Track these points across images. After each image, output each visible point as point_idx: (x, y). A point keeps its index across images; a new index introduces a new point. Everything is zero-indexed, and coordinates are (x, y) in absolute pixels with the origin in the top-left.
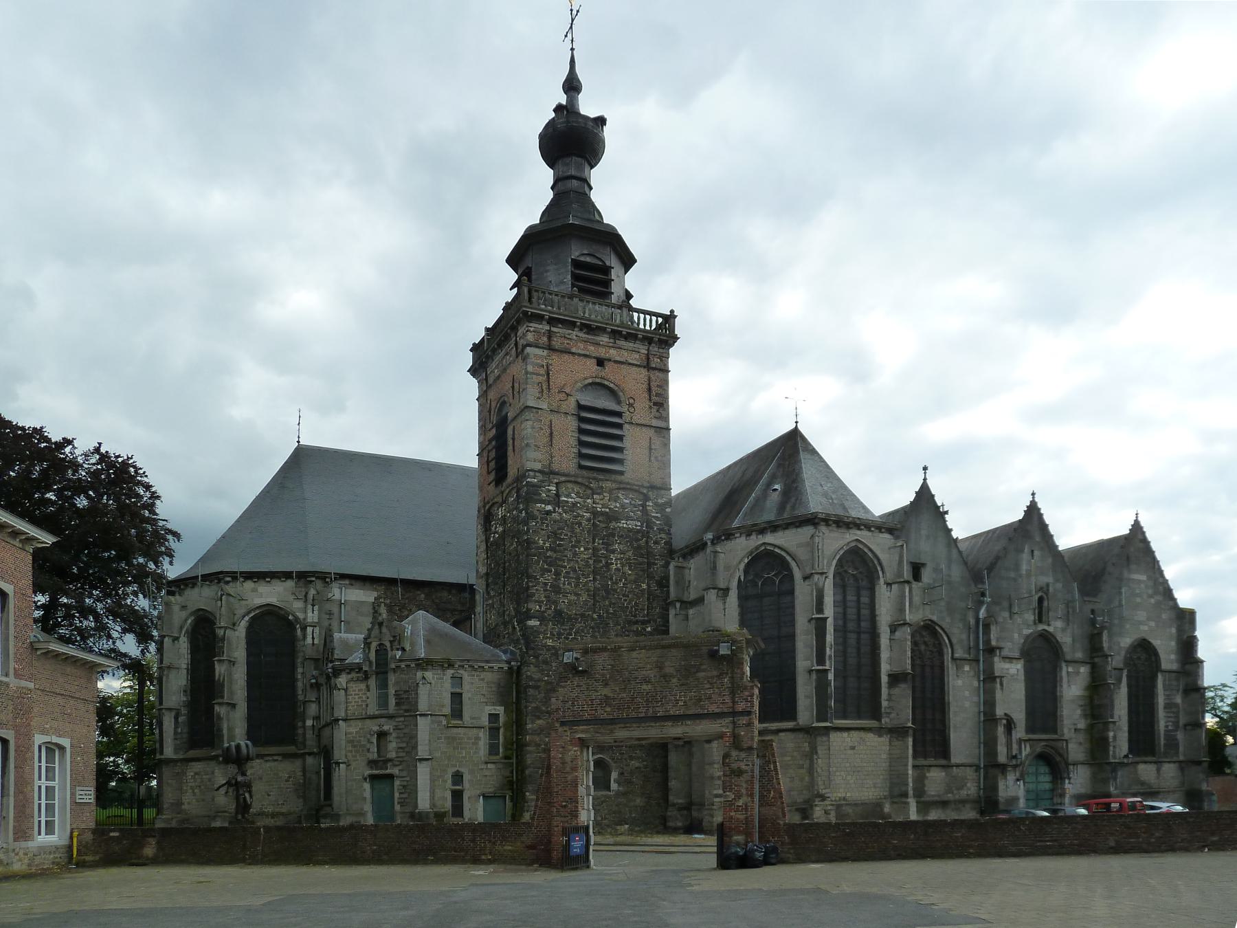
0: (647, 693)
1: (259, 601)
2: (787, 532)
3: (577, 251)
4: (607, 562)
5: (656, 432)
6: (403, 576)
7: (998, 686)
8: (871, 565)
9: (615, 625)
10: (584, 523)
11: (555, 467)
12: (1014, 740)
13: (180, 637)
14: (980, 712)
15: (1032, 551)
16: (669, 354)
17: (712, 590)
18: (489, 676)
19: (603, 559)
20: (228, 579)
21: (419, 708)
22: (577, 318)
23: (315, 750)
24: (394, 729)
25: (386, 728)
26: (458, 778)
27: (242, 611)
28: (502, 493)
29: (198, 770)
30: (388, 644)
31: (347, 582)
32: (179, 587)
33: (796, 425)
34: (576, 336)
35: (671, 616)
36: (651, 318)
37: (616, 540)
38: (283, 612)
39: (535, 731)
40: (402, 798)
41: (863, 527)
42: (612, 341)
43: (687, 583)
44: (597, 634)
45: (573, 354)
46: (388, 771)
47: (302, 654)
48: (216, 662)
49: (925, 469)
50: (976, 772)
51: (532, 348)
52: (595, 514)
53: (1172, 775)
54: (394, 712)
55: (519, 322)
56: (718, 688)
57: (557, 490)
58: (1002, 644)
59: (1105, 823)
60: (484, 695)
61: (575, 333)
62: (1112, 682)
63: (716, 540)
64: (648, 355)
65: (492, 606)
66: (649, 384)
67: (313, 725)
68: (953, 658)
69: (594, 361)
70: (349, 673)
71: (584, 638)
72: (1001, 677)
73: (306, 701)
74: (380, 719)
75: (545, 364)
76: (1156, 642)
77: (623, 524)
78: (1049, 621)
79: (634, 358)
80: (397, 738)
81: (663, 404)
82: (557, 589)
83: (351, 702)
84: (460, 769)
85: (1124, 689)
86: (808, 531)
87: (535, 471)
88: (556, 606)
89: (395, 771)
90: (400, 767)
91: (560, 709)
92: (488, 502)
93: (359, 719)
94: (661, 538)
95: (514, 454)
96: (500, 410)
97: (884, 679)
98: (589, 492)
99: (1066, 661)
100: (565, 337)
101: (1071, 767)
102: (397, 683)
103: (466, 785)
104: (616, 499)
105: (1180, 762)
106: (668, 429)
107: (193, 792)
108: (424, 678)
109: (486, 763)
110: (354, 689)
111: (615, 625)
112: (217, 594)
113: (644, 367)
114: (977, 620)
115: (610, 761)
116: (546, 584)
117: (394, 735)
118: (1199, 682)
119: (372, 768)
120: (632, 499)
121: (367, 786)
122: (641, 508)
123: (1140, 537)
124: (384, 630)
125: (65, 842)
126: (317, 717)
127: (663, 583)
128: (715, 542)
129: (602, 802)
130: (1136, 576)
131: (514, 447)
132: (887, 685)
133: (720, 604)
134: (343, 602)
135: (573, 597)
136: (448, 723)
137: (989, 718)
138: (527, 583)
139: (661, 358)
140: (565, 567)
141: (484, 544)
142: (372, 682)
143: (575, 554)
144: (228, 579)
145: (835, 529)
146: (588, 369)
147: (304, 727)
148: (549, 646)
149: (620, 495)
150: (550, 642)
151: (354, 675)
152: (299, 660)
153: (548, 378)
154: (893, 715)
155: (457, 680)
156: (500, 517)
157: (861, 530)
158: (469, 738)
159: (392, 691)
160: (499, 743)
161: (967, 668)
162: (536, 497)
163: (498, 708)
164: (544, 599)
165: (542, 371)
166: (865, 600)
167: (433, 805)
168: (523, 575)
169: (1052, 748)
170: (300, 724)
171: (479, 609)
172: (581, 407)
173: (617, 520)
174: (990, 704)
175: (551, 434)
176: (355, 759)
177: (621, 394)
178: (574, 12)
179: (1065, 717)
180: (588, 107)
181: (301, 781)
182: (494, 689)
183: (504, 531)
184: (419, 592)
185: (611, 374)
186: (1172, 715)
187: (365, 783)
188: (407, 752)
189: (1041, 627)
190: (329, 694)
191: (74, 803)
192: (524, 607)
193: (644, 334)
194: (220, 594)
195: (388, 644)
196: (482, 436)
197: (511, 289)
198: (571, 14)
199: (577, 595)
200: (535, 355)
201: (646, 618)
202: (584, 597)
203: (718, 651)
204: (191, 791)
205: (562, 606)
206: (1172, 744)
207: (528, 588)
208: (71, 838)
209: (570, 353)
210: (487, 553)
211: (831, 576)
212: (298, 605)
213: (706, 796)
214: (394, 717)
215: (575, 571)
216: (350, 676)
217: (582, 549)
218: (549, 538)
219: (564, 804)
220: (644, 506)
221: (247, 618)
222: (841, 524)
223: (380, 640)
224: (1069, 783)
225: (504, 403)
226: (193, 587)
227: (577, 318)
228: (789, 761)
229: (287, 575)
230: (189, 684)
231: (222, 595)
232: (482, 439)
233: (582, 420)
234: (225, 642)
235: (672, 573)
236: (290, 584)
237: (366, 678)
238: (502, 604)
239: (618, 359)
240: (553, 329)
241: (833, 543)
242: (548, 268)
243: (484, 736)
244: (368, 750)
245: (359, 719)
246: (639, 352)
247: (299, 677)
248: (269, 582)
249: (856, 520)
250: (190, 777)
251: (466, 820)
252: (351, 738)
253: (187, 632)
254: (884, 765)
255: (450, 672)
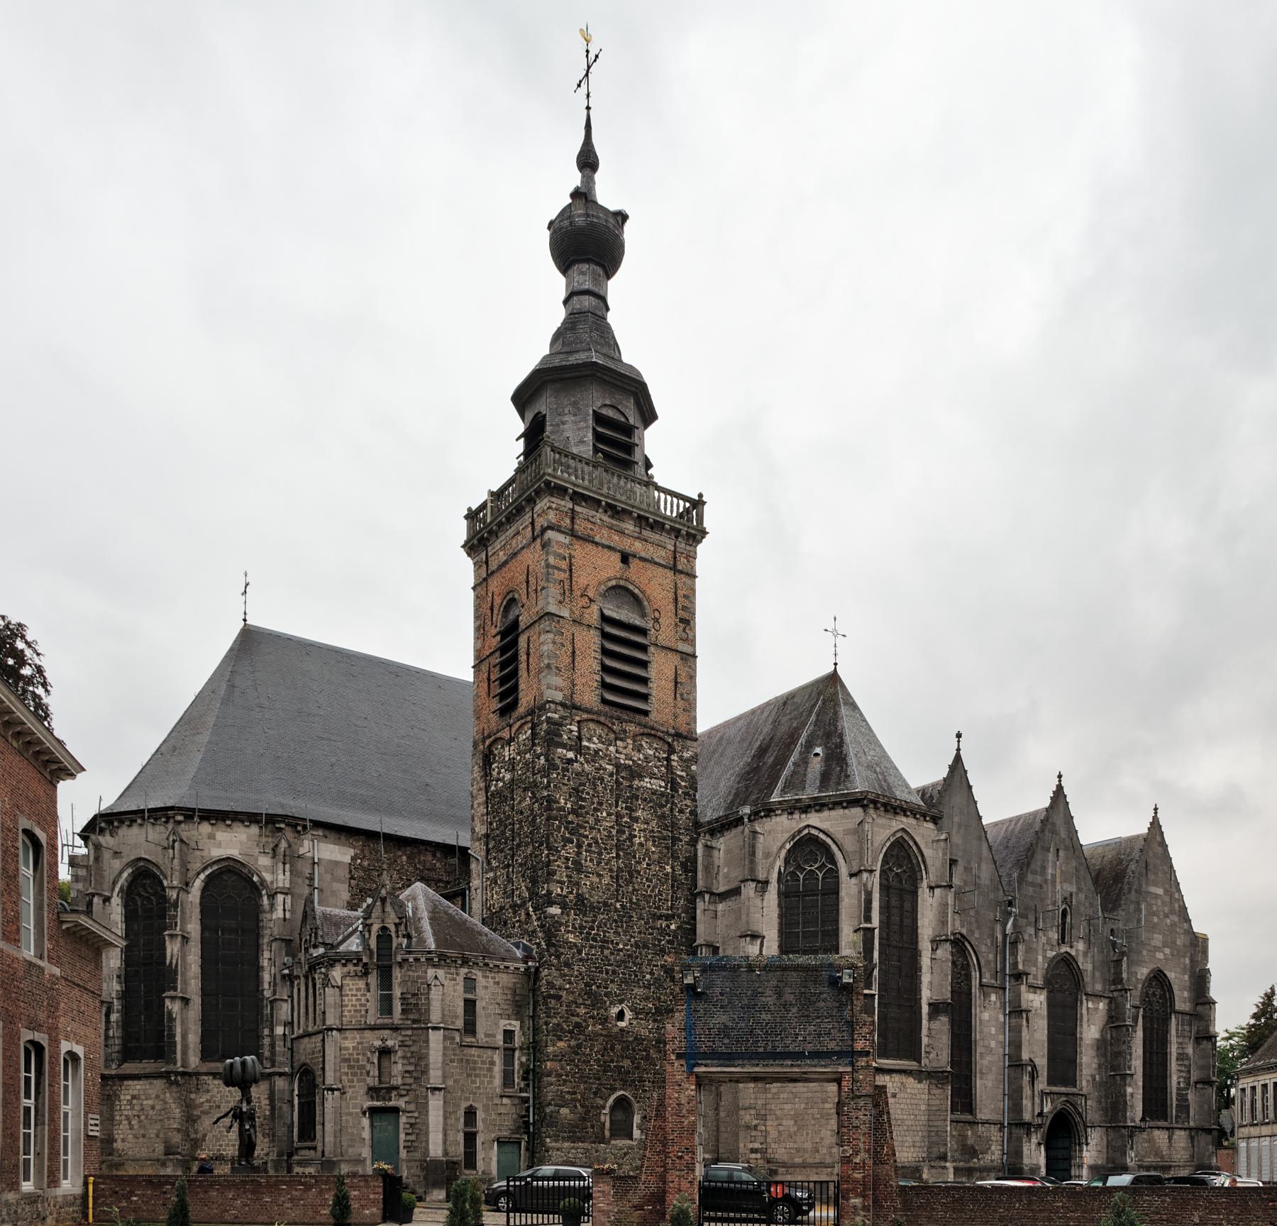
0: (767, 1023)
1: (217, 853)
2: (833, 813)
3: (595, 399)
4: (630, 834)
5: (682, 659)
6: (386, 830)
7: (1024, 1022)
8: (914, 861)
9: (639, 919)
10: (607, 778)
11: (577, 699)
12: (1036, 1093)
13: (112, 896)
14: (1005, 1055)
15: (1058, 850)
16: (696, 553)
17: (751, 883)
18: (505, 979)
19: (626, 829)
20: (180, 818)
21: (431, 1017)
22: (602, 495)
23: (287, 1069)
24: (399, 1046)
25: (390, 1043)
26: (470, 1114)
27: (197, 866)
28: (511, 726)
29: (136, 1092)
30: (392, 928)
31: (320, 833)
32: (110, 823)
33: (835, 668)
34: (600, 520)
35: (698, 912)
36: (666, 498)
37: (640, 805)
38: (246, 871)
39: (556, 1056)
40: (409, 1141)
41: (909, 813)
42: (637, 529)
43: (716, 869)
44: (620, 930)
45: (597, 544)
46: (392, 1104)
47: (268, 931)
48: (167, 938)
49: (959, 736)
50: (1000, 1131)
51: (554, 532)
52: (618, 766)
53: (1182, 1145)
54: (400, 1022)
55: (538, 492)
56: (838, 1022)
57: (579, 731)
58: (1027, 970)
59: (1190, 1196)
60: (499, 1004)
61: (599, 516)
62: (1131, 1023)
63: (755, 816)
64: (675, 552)
65: (494, 881)
66: (676, 593)
67: (284, 1034)
68: (981, 985)
69: (618, 556)
70: (344, 965)
71: (607, 934)
72: (1028, 1011)
73: (276, 1000)
74: (382, 1031)
75: (567, 555)
76: (1171, 975)
77: (647, 783)
78: (1071, 942)
79: (660, 555)
80: (404, 1057)
81: (689, 621)
82: (578, 867)
83: (347, 1006)
84: (473, 1104)
85: (1140, 1034)
86: (857, 812)
87: (556, 703)
88: (578, 889)
89: (401, 1103)
90: (406, 1099)
91: (676, 1038)
92: (489, 736)
93: (356, 1029)
94: (686, 805)
95: (529, 676)
96: (507, 609)
97: (925, 1009)
98: (612, 736)
99: (1086, 994)
100: (588, 520)
101: (1089, 1130)
102: (404, 982)
103: (480, 1125)
104: (639, 749)
105: (1190, 1129)
106: (694, 656)
107: (130, 1123)
108: (436, 977)
109: (502, 1097)
110: (351, 986)
111: (639, 919)
112: (168, 839)
113: (671, 569)
114: (1005, 936)
115: (632, 1099)
116: (567, 859)
117: (400, 1054)
118: (1211, 1029)
119: (372, 1099)
120: (656, 749)
121: (366, 1122)
122: (665, 762)
123: (1159, 839)
124: (388, 908)
125: (78, 1190)
126: (289, 1023)
127: (690, 866)
128: (752, 818)
129: (626, 1154)
130: (1153, 889)
131: (528, 665)
132: (927, 1017)
133: (758, 902)
134: (316, 861)
135: (596, 879)
136: (461, 1041)
137: (1016, 1064)
138: (547, 856)
139: (688, 557)
140: (586, 837)
141: (483, 792)
142: (373, 979)
143: (597, 820)
144: (180, 818)
145: (882, 814)
146: (610, 566)
147: (272, 1035)
148: (571, 942)
149: (643, 743)
150: (571, 938)
151: (351, 967)
152: (266, 940)
153: (571, 576)
154: (932, 1056)
155: (470, 984)
156: (507, 759)
157: (907, 816)
158: (483, 1062)
159: (397, 992)
160: (513, 1070)
161: (993, 997)
162: (556, 739)
163: (513, 1022)
164: (566, 879)
165: (564, 565)
166: (907, 906)
167: (446, 1153)
168: (541, 844)
169: (1071, 1104)
170: (266, 1032)
171: (475, 883)
172: (605, 619)
173: (641, 777)
174: (1016, 1045)
175: (574, 652)
176: (352, 1084)
177: (646, 603)
178: (592, 56)
179: (192, 939)
180: (607, 195)
181: (267, 1113)
182: (509, 997)
183: (513, 780)
184: (400, 853)
185: (640, 576)
186: (1183, 1068)
187: (364, 1119)
188: (415, 1078)
189: (1064, 949)
190: (311, 991)
191: (88, 1137)
192: (543, 887)
193: (672, 524)
194: (171, 839)
195: (392, 928)
196: (479, 641)
197: (517, 440)
198: (587, 56)
199: (599, 875)
200: (558, 542)
201: (670, 912)
202: (606, 880)
203: (840, 978)
204: (126, 1122)
205: (584, 890)
206: (1184, 1107)
207: (549, 863)
208: (86, 1184)
209: (593, 542)
210: (487, 807)
211: (878, 873)
212: (264, 861)
213: (741, 1151)
214: (400, 1029)
215: (597, 842)
216: (345, 970)
217: (604, 814)
218: (570, 796)
219: (680, 1154)
220: (668, 759)
221: (202, 876)
222: (889, 808)
223: (383, 921)
224: (1087, 1151)
225: (513, 600)
226: (130, 826)
227: (602, 495)
228: (830, 1109)
229: (251, 818)
230: (123, 966)
231: (174, 841)
232: (479, 646)
233: (605, 636)
234: (179, 910)
235: (700, 853)
236: (254, 830)
237: (366, 974)
238: (510, 880)
239: (643, 554)
240: (577, 508)
241: (883, 830)
242: (566, 418)
243: (498, 1058)
244: (368, 1073)
245: (356, 1029)
246: (665, 548)
247: (265, 963)
248: (229, 826)
249: (903, 803)
250: (125, 1102)
251: (480, 1173)
252: (347, 1056)
253: (121, 890)
254: (923, 1118)
255: (464, 971)
